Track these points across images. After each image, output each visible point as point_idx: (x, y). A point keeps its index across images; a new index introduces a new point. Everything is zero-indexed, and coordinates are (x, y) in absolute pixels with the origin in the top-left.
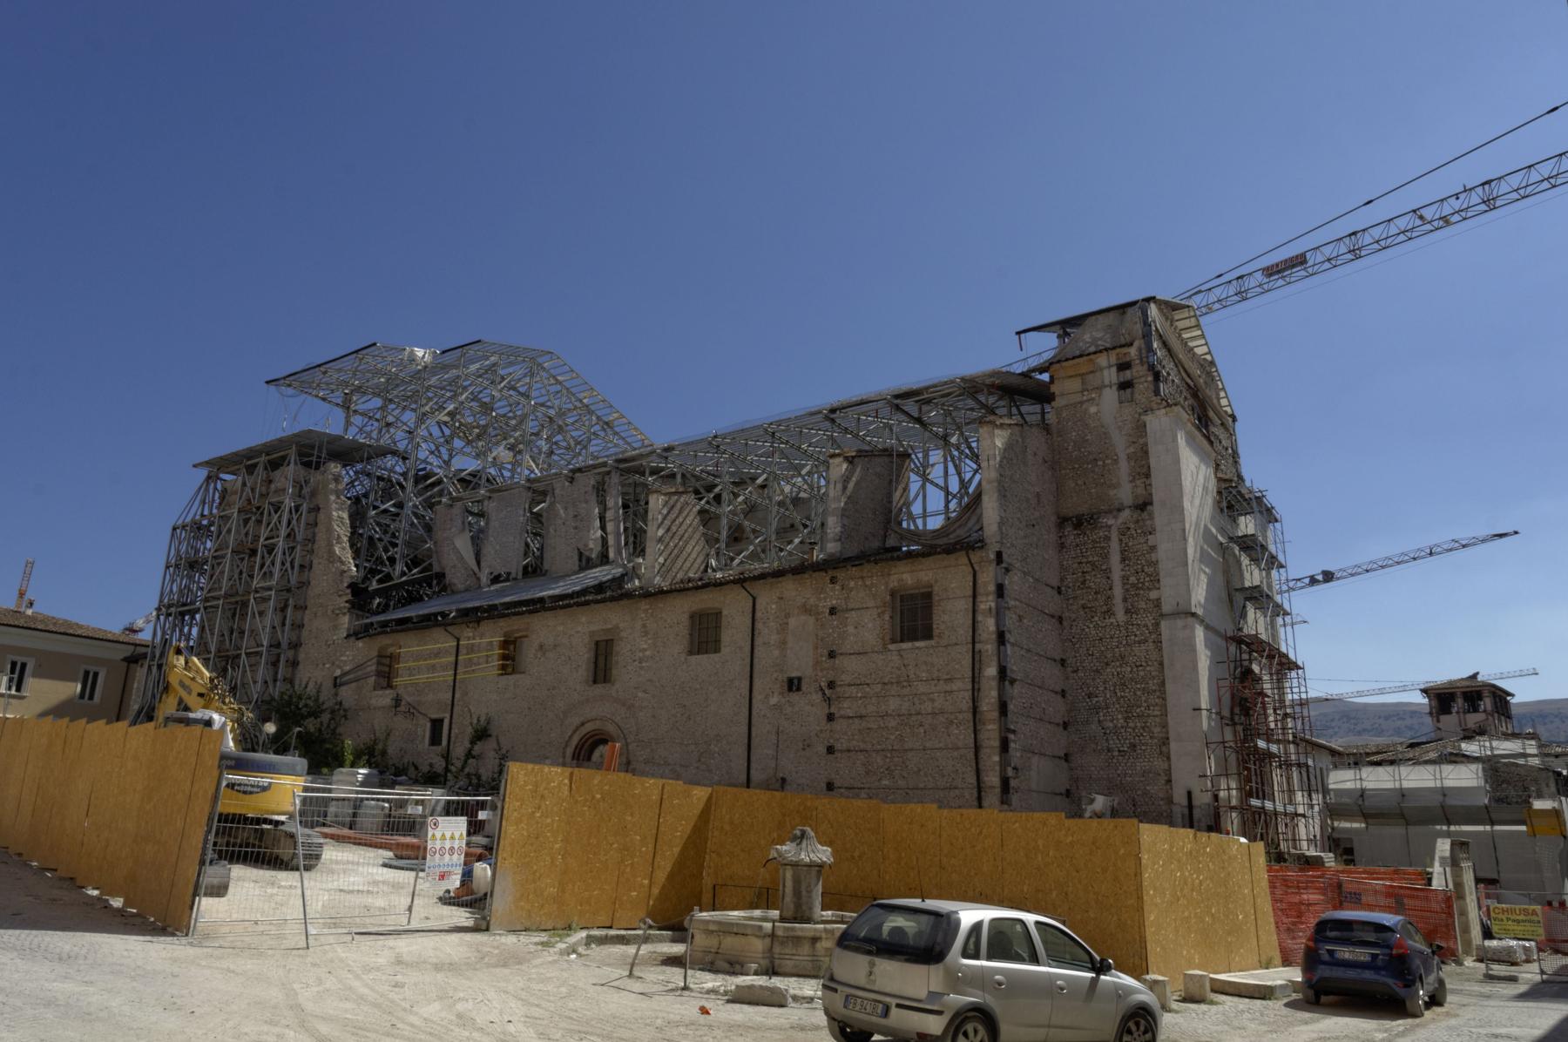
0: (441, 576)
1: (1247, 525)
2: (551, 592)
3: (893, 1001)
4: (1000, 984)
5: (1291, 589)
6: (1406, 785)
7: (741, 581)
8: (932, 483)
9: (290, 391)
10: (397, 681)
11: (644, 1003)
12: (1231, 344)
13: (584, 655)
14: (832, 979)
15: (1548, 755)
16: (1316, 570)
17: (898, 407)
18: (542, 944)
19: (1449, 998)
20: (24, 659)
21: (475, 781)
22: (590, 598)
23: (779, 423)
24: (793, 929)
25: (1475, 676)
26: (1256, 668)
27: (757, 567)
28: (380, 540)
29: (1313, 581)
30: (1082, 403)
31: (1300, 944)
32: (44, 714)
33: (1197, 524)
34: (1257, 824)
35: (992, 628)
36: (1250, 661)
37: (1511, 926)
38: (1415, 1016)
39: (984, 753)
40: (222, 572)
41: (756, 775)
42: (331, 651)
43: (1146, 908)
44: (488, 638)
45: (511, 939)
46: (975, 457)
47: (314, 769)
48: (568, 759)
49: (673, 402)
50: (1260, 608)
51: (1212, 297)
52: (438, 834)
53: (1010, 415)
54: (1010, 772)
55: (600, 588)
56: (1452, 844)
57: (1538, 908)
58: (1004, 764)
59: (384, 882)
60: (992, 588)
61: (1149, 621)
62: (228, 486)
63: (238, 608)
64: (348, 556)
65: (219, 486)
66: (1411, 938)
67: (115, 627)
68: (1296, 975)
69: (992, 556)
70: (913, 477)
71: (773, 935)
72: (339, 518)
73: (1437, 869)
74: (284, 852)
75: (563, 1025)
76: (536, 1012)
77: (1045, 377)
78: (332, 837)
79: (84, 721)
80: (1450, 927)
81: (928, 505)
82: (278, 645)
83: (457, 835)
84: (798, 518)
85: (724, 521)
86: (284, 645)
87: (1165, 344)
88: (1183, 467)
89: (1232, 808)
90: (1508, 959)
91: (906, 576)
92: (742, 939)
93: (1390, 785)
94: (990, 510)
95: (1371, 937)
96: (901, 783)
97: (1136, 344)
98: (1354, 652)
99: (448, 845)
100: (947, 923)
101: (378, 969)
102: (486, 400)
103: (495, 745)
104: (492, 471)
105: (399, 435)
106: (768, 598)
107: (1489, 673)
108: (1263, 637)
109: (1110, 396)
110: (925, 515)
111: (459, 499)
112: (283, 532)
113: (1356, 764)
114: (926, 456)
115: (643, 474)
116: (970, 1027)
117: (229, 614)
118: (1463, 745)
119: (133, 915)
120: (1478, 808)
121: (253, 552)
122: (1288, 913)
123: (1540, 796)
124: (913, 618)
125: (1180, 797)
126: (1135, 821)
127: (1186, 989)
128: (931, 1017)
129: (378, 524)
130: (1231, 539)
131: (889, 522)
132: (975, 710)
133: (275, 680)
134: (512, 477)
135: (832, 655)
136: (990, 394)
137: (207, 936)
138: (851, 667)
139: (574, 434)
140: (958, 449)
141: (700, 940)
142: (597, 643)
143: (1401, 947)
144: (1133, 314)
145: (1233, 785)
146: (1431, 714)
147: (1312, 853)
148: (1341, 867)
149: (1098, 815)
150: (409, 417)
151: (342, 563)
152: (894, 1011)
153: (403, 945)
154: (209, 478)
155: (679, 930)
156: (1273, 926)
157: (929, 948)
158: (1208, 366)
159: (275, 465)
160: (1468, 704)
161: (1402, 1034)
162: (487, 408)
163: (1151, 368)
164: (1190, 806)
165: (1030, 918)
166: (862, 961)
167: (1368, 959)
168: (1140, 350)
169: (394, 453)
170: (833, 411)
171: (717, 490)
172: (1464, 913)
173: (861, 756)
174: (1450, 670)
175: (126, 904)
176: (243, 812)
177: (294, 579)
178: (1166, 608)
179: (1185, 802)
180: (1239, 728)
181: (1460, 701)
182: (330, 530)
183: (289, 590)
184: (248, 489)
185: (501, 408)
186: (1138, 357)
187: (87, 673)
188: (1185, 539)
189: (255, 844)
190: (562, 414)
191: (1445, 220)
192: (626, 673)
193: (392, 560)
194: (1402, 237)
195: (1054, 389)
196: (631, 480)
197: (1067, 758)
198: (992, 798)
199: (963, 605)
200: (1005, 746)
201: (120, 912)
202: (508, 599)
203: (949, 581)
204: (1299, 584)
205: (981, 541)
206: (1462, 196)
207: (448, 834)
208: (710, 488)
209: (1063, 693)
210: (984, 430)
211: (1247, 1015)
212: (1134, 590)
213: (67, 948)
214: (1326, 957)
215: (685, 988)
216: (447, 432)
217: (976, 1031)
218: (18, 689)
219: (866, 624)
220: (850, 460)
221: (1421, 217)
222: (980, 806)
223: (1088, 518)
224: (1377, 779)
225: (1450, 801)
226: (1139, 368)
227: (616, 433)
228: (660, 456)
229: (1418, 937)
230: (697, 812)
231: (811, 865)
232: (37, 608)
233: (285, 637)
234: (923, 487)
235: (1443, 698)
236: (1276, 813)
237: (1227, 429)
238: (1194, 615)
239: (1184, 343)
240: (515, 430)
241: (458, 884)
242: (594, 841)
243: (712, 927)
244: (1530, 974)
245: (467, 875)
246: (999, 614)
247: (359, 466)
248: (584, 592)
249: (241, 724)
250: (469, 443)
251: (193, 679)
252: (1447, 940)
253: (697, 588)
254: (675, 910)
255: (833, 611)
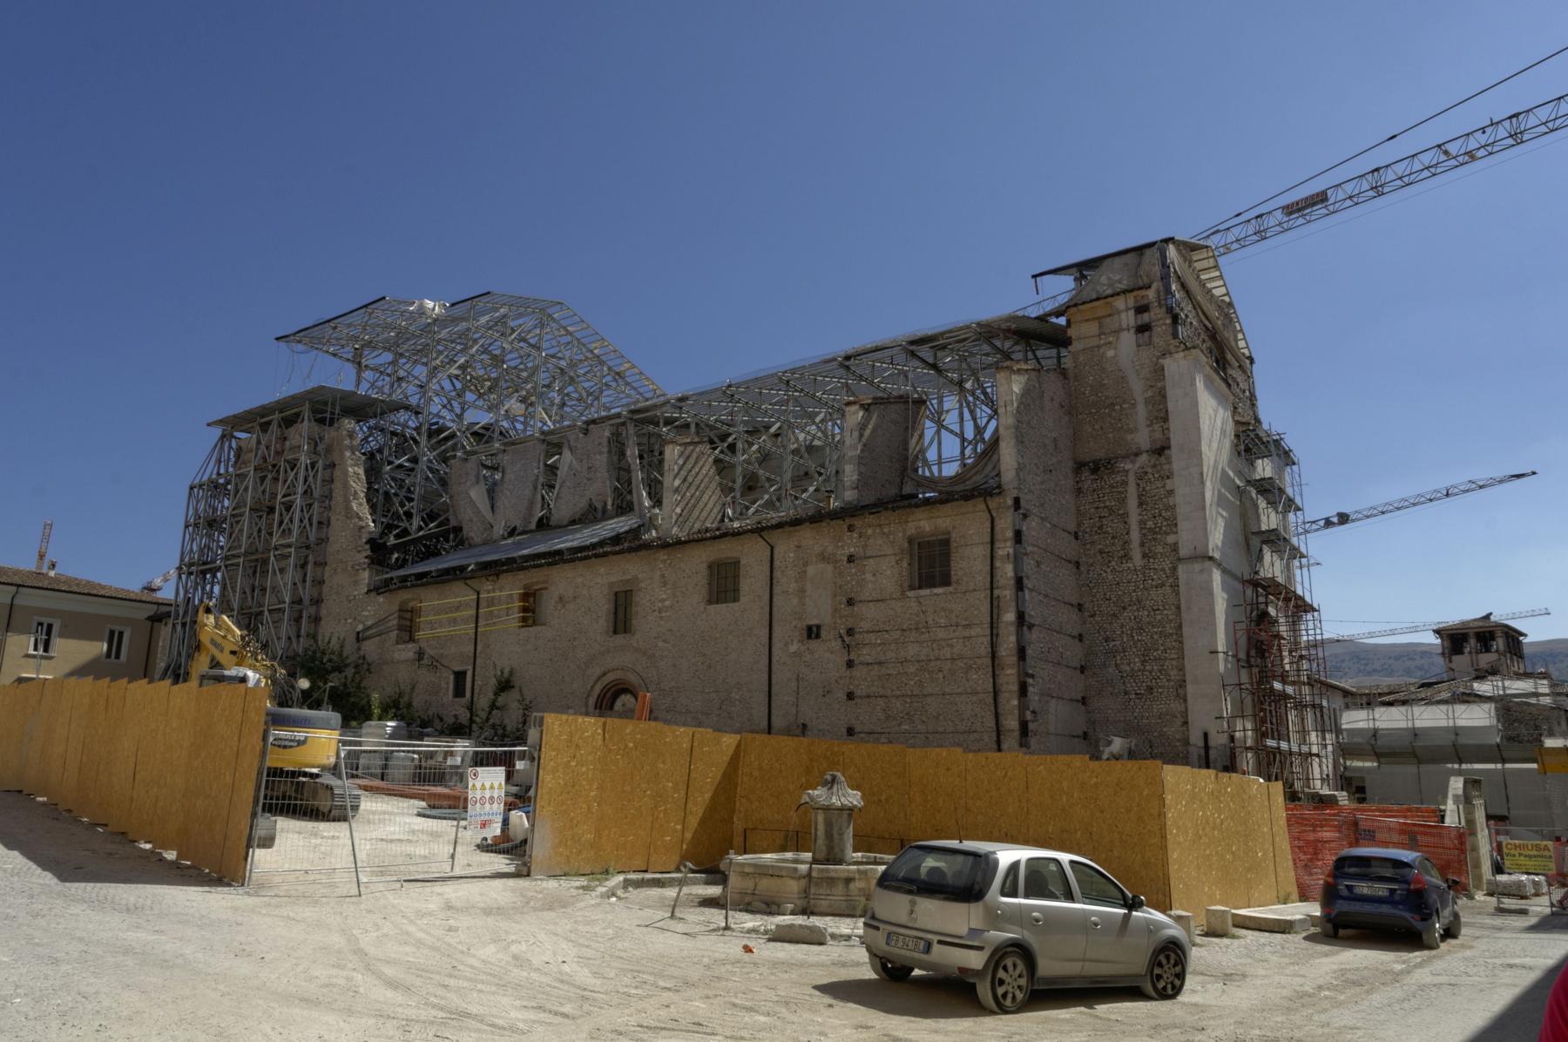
0: (458, 530)
1: (1264, 468)
2: (569, 545)
3: (935, 938)
4: (1037, 920)
5: (1307, 532)
6: (1418, 724)
7: (759, 530)
8: (946, 429)
9: (300, 347)
10: (420, 635)
11: (689, 944)
12: (1252, 287)
13: (604, 607)
14: (873, 917)
15: (1559, 694)
16: (1331, 512)
17: (913, 354)
18: (583, 888)
19: (1464, 931)
20: (50, 620)
21: (500, 732)
22: (608, 549)
23: (793, 371)
24: (827, 871)
25: (1488, 617)
26: (1272, 611)
27: (773, 516)
28: (396, 495)
29: (1328, 523)
30: (1099, 347)
31: (1319, 880)
32: (71, 674)
33: (1215, 468)
34: (1272, 764)
35: (1011, 574)
36: (1267, 604)
37: (1522, 860)
38: (1430, 948)
39: (1003, 698)
40: (241, 530)
41: (777, 722)
42: (352, 606)
43: (1170, 846)
44: (508, 590)
45: (552, 884)
46: (990, 402)
47: (346, 724)
48: (591, 708)
49: (682, 358)
50: (1277, 551)
51: (1231, 237)
52: (478, 785)
53: (1026, 360)
54: (1029, 716)
55: (616, 539)
56: (1465, 782)
57: (1550, 844)
58: (1022, 708)
59: (422, 831)
60: (1010, 534)
61: (1167, 565)
62: (242, 444)
63: (258, 566)
64: (365, 512)
65: (234, 444)
66: (1428, 873)
67: (134, 586)
68: (1315, 910)
69: (1010, 502)
70: (928, 423)
71: (809, 875)
72: (355, 473)
73: (1450, 806)
74: (324, 804)
75: (614, 964)
76: (589, 953)
77: (1062, 321)
78: (366, 788)
79: (125, 680)
80: (1462, 862)
81: (944, 452)
82: (300, 601)
83: (496, 785)
84: (812, 466)
85: (739, 470)
86: (306, 601)
87: (1183, 286)
88: (1202, 410)
89: (1247, 749)
90: (1518, 892)
91: (924, 523)
92: (779, 881)
93: (1403, 725)
94: (1008, 456)
95: (1388, 873)
96: (921, 727)
97: (1155, 286)
98: (1369, 594)
99: (488, 794)
100: (985, 864)
101: (430, 914)
102: (497, 352)
103: (518, 696)
104: (505, 424)
105: (411, 389)
106: (785, 547)
107: (1501, 613)
108: (1280, 580)
109: (1128, 340)
110: (940, 463)
111: (475, 453)
112: (300, 490)
113: (1369, 704)
114: (941, 402)
115: (657, 424)
116: (1009, 962)
117: (250, 572)
118: (1475, 685)
119: (188, 867)
120: (1491, 746)
121: (271, 510)
122: (1306, 851)
123: (1551, 735)
124: (931, 565)
125: (1196, 739)
126: (1159, 762)
127: (1209, 923)
128: (972, 953)
129: (394, 479)
130: (1249, 482)
131: (905, 469)
132: (994, 656)
133: (298, 636)
134: (525, 430)
135: (850, 602)
136: (1006, 338)
137: (261, 886)
138: (869, 615)
139: (586, 385)
140: (973, 394)
141: (734, 880)
142: (616, 594)
143: (1418, 881)
144: (1151, 256)
145: (1249, 726)
146: (1443, 654)
147: (1326, 791)
148: (1355, 805)
149: (1117, 758)
150: (421, 372)
151: (360, 519)
152: (936, 948)
153: (450, 891)
154: (223, 436)
155: (715, 874)
156: (1291, 863)
157: (969, 886)
158: (1226, 308)
159: (289, 422)
160: (1480, 644)
161: (1420, 965)
162: (497, 360)
163: (1170, 310)
164: (1207, 747)
165: (1065, 857)
166: (902, 900)
167: (1386, 893)
168: (1158, 291)
169: (407, 408)
170: (848, 358)
171: (730, 439)
172: (1475, 849)
173: (881, 702)
174: (1463, 611)
175: (179, 856)
176: (279, 765)
177: (312, 537)
178: (1183, 552)
179: (1201, 743)
180: (1255, 670)
181: (1473, 641)
182: (346, 485)
183: (308, 547)
184: (263, 447)
185: (512, 361)
186: (1157, 298)
187: (112, 633)
188: (1203, 483)
189: (297, 797)
190: (573, 365)
191: (1471, 156)
192: (646, 621)
193: (409, 515)
194: (1426, 173)
195: (1071, 332)
196: (644, 432)
197: (1084, 701)
198: (1011, 741)
199: (981, 551)
200: (1023, 690)
201: (175, 865)
202: (525, 552)
203: (967, 528)
204: (1314, 527)
205: (999, 486)
206: (1489, 130)
207: (489, 783)
208: (724, 437)
209: (1080, 637)
210: (1001, 376)
211: (1268, 948)
212: (1151, 535)
213: (132, 899)
214: (1345, 893)
215: (727, 928)
216: (459, 385)
217: (1015, 966)
218: (46, 650)
219: (885, 570)
220: (866, 408)
221: (1446, 152)
222: (999, 750)
223: (1105, 462)
224: (1390, 719)
225: (1462, 740)
226: (1157, 310)
227: (627, 384)
228: (674, 406)
229: (1434, 872)
230: (726, 759)
231: (842, 809)
232: (58, 570)
233: (306, 593)
234: (938, 432)
235: (1455, 639)
236: (1291, 753)
237: (1244, 371)
238: (1211, 558)
239: (1202, 284)
240: (526, 382)
241: (498, 832)
242: (627, 788)
243: (747, 870)
244: (1541, 907)
245: (506, 822)
246: (1017, 560)
247: (372, 422)
248: (601, 543)
249: (274, 682)
250: (481, 396)
251: (224, 637)
252: (1459, 874)
253: (715, 538)
254: (712, 853)
255: (851, 559)
